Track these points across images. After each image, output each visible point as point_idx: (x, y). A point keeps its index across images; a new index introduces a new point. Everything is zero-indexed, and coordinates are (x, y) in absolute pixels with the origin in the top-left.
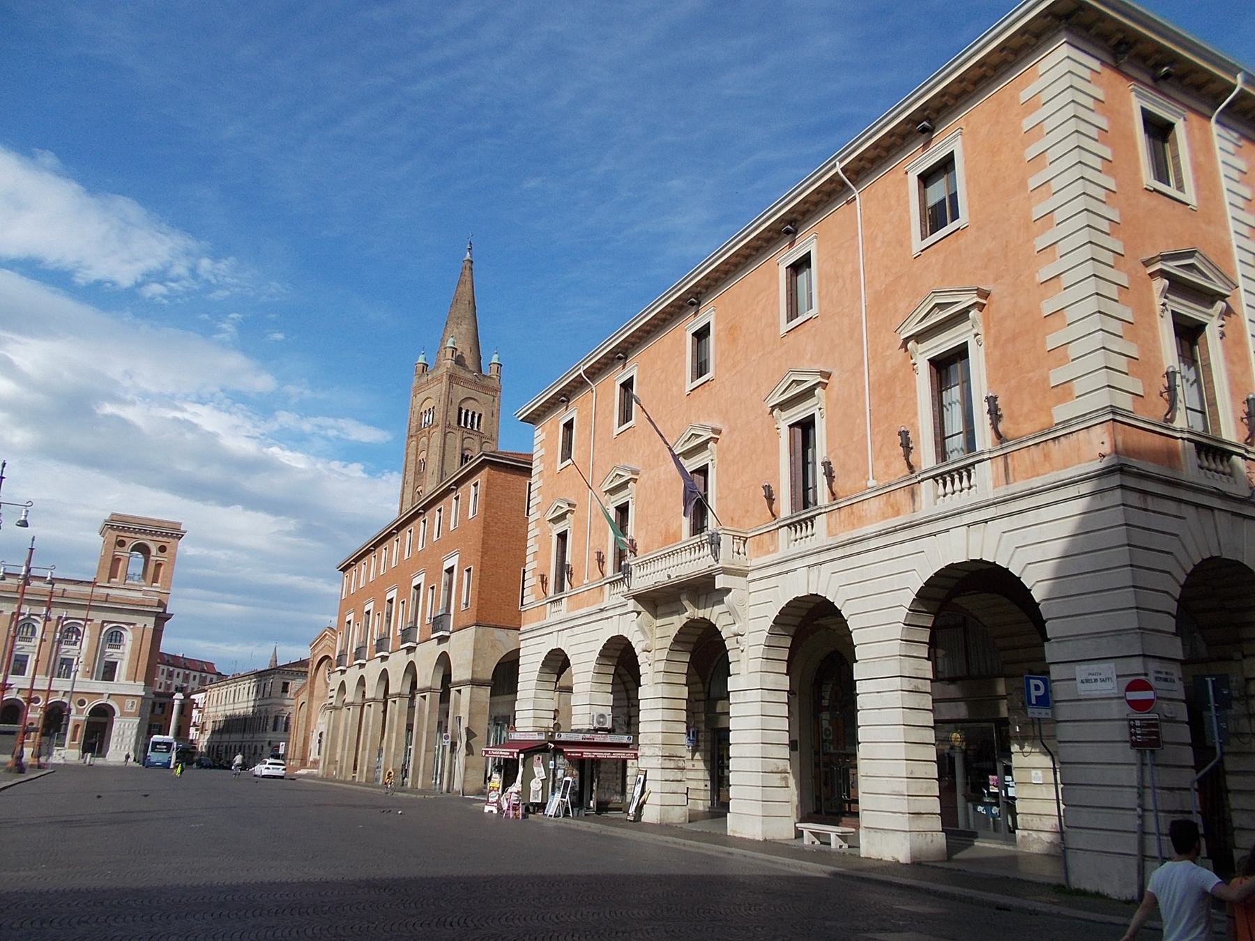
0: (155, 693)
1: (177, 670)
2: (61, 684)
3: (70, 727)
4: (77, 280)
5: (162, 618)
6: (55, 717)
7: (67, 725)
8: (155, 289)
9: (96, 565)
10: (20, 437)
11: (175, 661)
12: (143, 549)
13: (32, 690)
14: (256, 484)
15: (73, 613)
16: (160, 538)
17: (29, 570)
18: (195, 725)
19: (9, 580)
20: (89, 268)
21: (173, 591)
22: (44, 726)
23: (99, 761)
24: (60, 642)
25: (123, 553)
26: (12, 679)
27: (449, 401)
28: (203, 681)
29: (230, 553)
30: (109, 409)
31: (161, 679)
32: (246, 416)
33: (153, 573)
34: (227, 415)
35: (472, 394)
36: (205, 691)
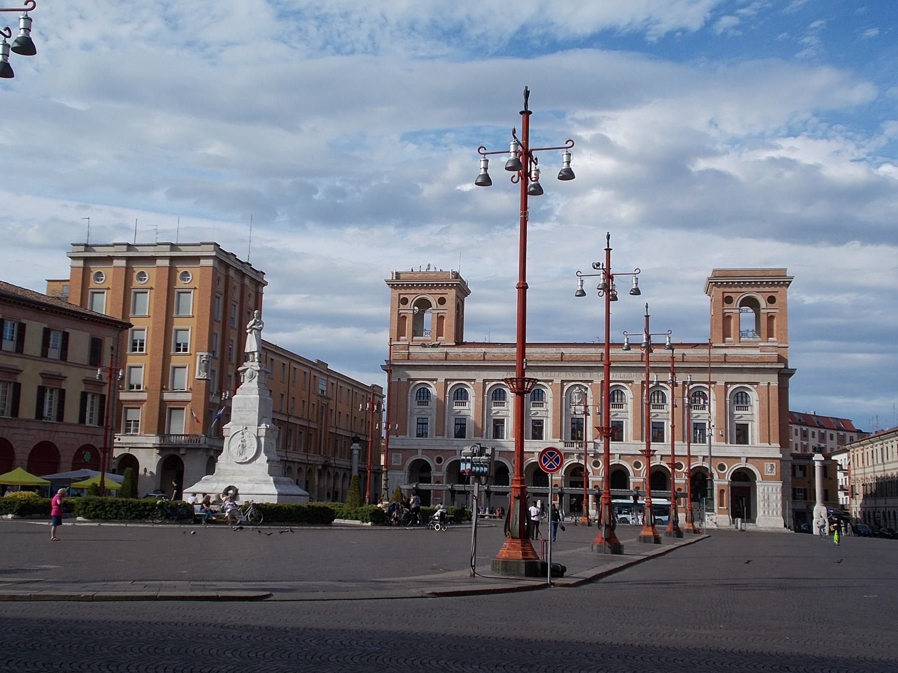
0: (792, 455)
1: (811, 430)
2: (698, 449)
3: (716, 492)
4: (650, 39)
5: (785, 375)
6: (700, 481)
7: (712, 490)
8: (727, 21)
9: (708, 327)
10: (627, 211)
11: (806, 420)
13: (673, 456)
14: (872, 213)
15: (696, 377)
17: (648, 338)
18: (842, 489)
19: (633, 350)
20: (658, 22)
21: (792, 345)
22: (691, 491)
23: (749, 527)
24: (689, 406)
25: (732, 309)
26: (654, 446)
28: (842, 441)
29: (853, 296)
30: (702, 164)
31: (795, 440)
32: (847, 138)
33: (767, 326)
34: (824, 141)
36: (846, 451)
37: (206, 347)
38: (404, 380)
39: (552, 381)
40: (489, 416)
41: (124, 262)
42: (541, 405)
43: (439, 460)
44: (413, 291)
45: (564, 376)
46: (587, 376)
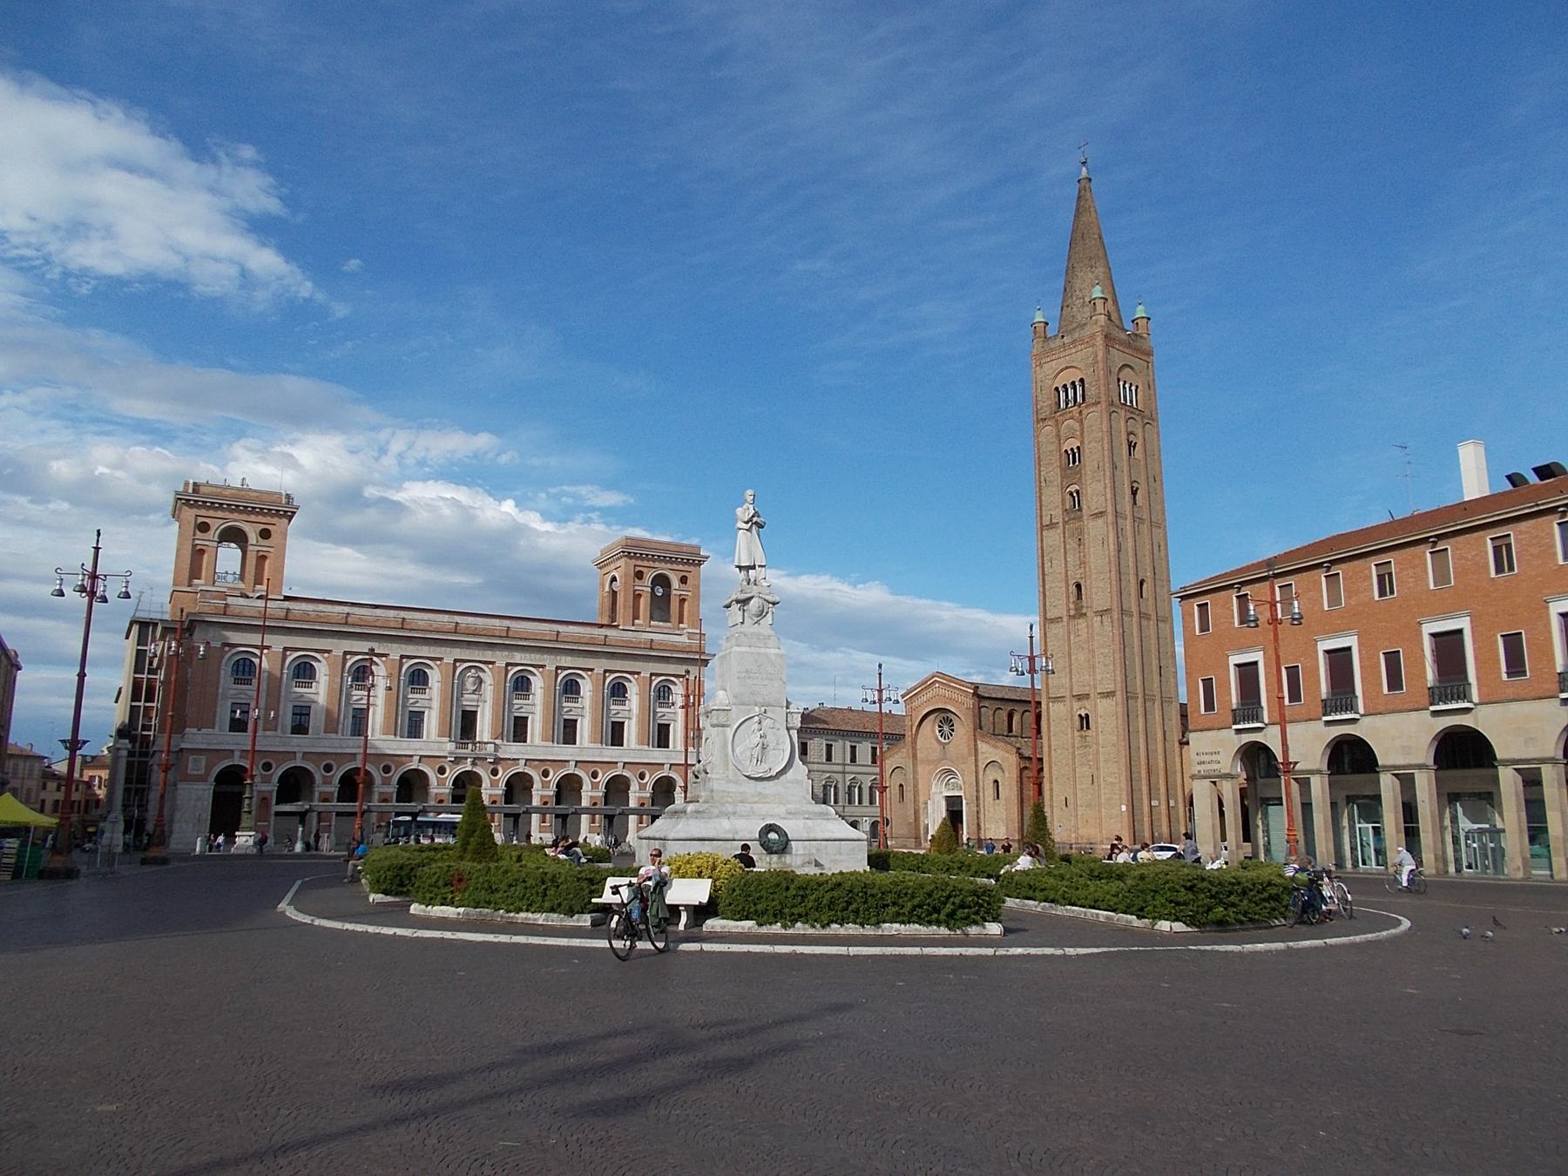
12: (234, 535)
39: (440, 659)
40: (348, 703)
42: (526, 697)
43: (328, 768)
44: (220, 514)
46: (488, 655)
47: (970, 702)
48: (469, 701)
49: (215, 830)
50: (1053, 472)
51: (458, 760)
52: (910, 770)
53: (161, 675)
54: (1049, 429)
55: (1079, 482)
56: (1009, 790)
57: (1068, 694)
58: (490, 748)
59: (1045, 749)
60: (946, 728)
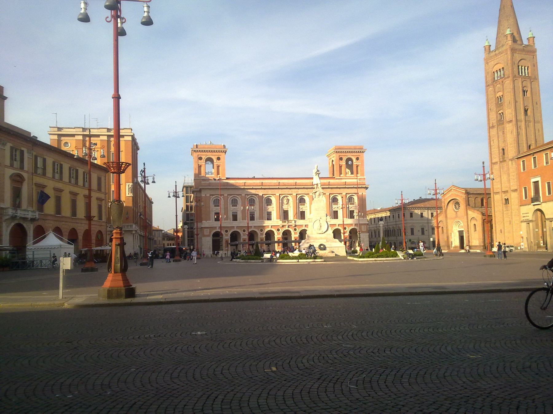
12: (210, 160)
13: (344, 224)
16: (356, 154)
25: (202, 162)
27: (513, 64)
35: (523, 56)
37: (131, 180)
38: (208, 195)
41: (82, 136)
42: (304, 205)
45: (280, 192)
46: (290, 191)
47: (464, 196)
48: (285, 207)
49: (214, 250)
50: (493, 106)
51: (283, 226)
52: (445, 222)
53: (193, 204)
54: (491, 89)
55: (502, 109)
56: (479, 228)
57: (500, 191)
58: (293, 222)
59: (493, 212)
60: (457, 206)
